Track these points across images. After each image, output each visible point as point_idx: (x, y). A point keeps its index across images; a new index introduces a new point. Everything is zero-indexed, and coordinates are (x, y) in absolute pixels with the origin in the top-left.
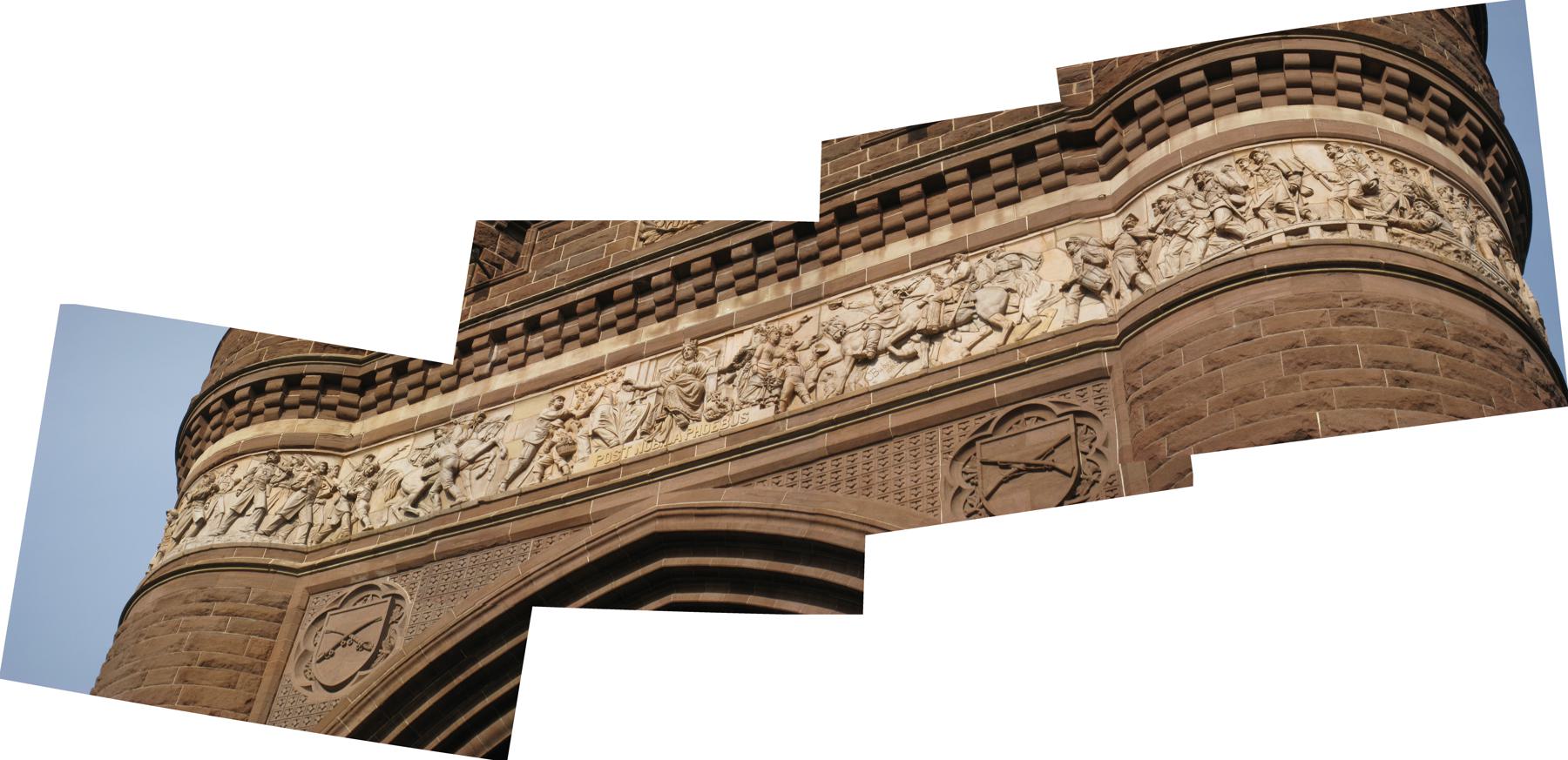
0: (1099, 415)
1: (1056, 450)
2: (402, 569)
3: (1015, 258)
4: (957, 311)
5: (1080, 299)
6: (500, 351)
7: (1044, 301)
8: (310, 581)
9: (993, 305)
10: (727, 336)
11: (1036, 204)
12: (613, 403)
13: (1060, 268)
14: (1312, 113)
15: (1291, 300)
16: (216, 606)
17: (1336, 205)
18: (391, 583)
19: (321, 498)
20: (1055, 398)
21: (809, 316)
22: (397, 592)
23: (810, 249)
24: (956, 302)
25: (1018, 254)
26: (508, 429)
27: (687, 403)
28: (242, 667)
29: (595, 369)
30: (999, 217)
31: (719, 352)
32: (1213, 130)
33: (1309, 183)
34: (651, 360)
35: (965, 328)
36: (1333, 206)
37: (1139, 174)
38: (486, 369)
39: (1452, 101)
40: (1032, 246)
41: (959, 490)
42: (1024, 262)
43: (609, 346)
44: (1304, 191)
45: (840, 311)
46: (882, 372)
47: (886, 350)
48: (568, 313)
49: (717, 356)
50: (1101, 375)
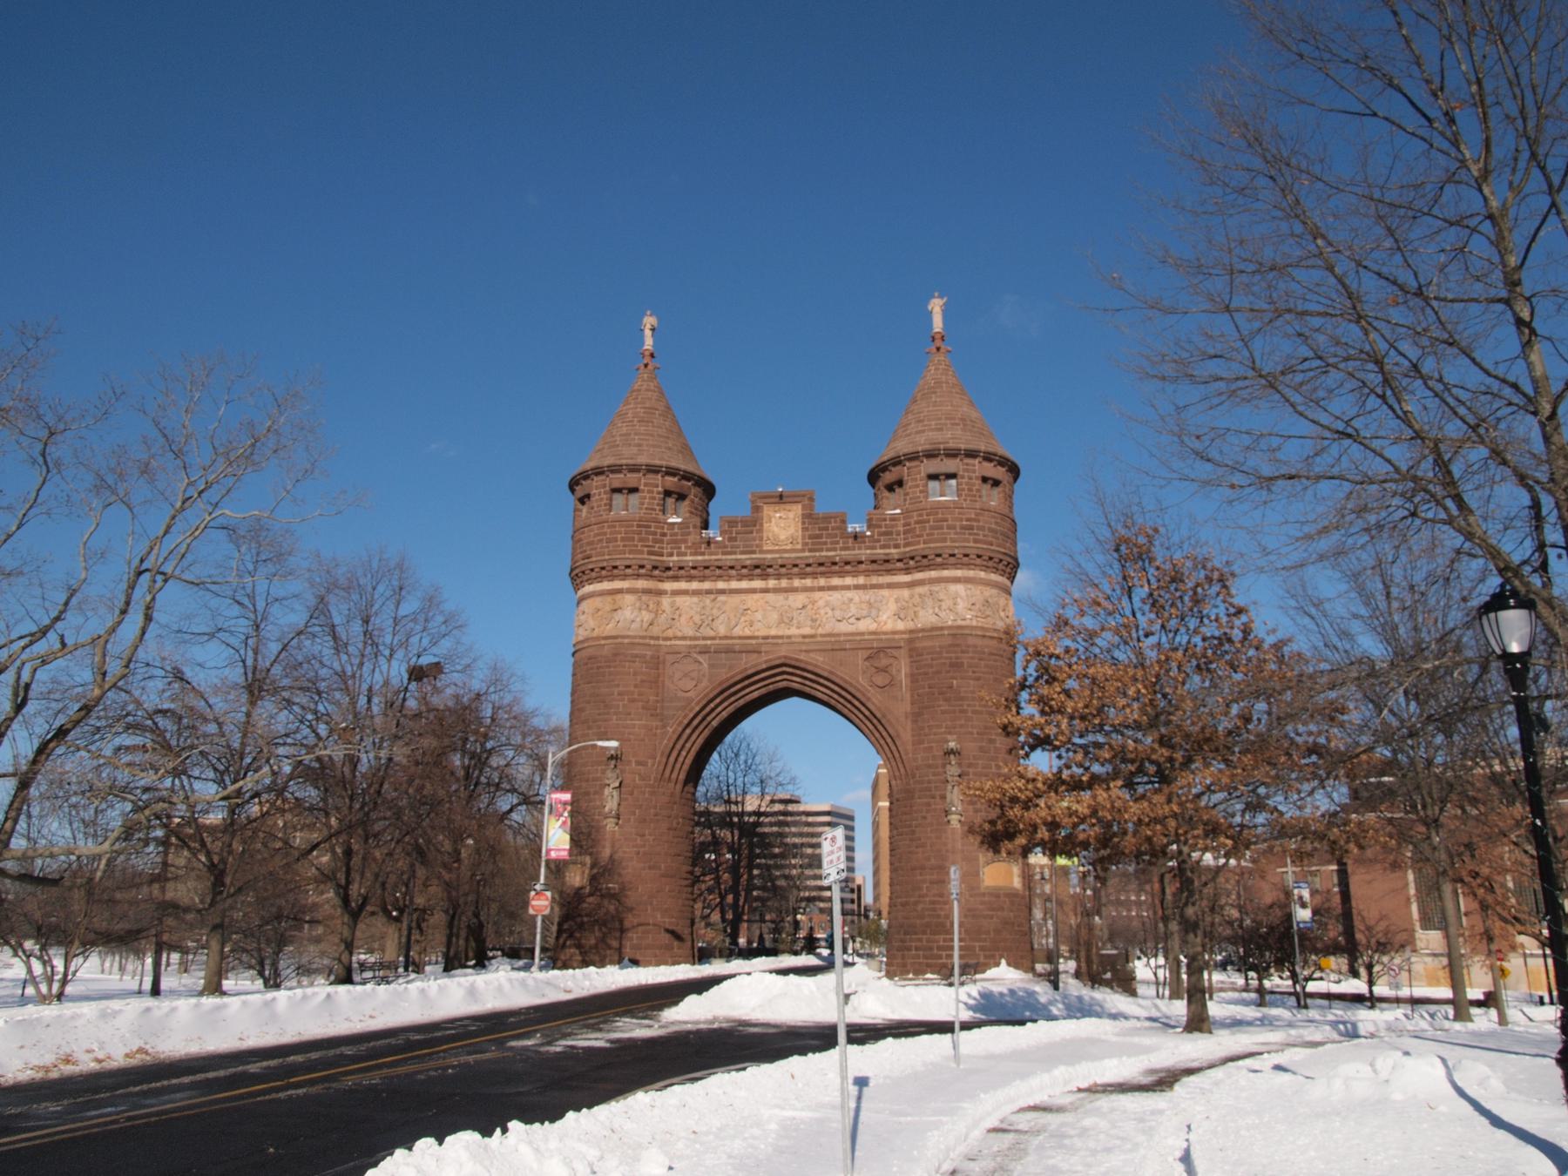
13: (893, 607)
29: (753, 591)
40: (885, 592)
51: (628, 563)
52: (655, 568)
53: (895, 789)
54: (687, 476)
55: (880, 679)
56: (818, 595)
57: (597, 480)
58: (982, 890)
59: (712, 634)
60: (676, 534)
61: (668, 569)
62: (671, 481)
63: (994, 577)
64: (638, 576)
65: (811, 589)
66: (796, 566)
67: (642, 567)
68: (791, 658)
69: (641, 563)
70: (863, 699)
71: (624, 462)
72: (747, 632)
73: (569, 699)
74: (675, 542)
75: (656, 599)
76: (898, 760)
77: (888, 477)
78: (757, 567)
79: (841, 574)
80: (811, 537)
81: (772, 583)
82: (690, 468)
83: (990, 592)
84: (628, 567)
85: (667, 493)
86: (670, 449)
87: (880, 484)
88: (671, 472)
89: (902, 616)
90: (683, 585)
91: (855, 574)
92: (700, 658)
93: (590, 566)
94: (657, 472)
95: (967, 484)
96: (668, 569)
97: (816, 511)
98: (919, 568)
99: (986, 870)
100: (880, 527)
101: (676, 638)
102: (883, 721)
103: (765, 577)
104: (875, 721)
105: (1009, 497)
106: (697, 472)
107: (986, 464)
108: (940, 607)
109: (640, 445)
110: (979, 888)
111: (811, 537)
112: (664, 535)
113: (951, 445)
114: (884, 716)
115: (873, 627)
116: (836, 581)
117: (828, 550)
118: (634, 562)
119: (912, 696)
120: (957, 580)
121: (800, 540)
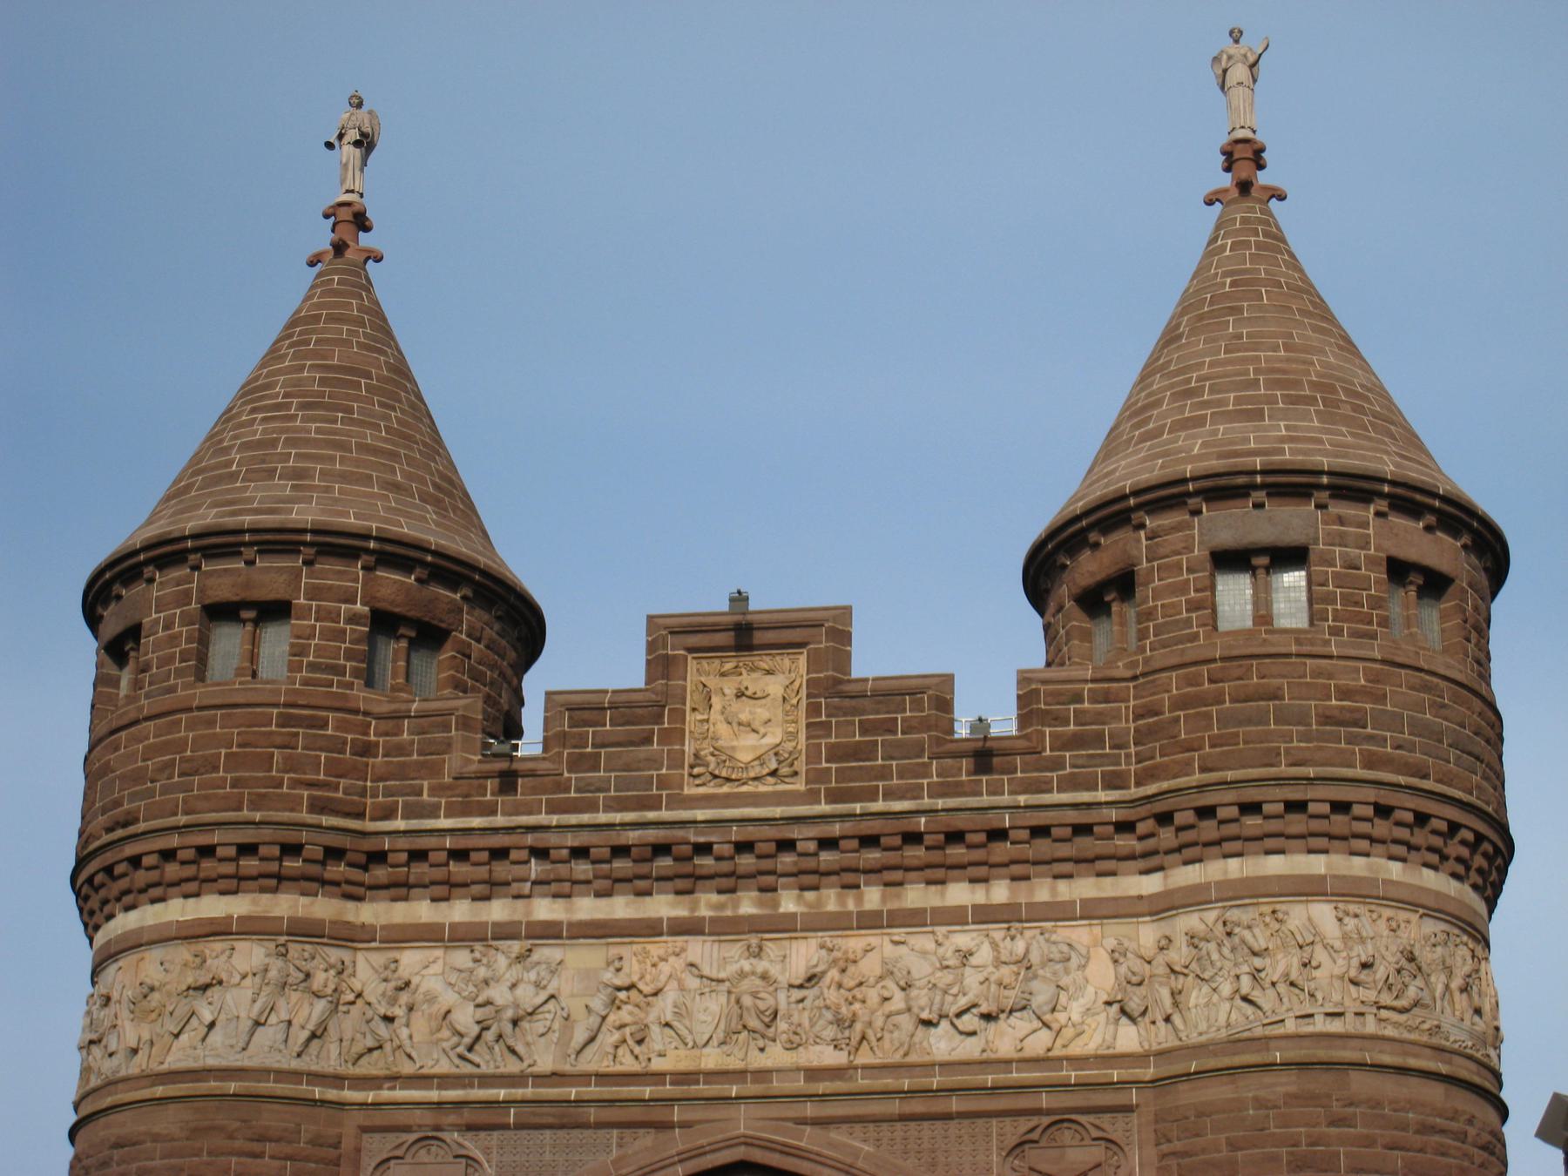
0: (1126, 1149)
1: (220, 881)
2: (471, 1128)
3: (1065, 948)
4: (1011, 997)
5: (1119, 1019)
6: (539, 869)
7: (1088, 1009)
9: (1046, 1003)
10: (791, 938)
12: (682, 988)
13: (1101, 977)
18: (460, 1140)
19: (345, 1004)
20: (1092, 1118)
21: (873, 945)
22: (471, 1154)
23: (873, 862)
24: (1014, 988)
25: (1069, 945)
27: (763, 1022)
30: (1053, 890)
31: (785, 957)
33: (1320, 955)
34: (714, 941)
35: (1017, 1014)
36: (1336, 985)
37: (1180, 889)
38: (527, 887)
39: (1494, 851)
40: (1080, 934)
42: (1073, 954)
43: (663, 906)
45: (903, 949)
47: (947, 1016)
48: (620, 851)
49: (783, 961)
50: (1128, 1109)
121: (801, 766)
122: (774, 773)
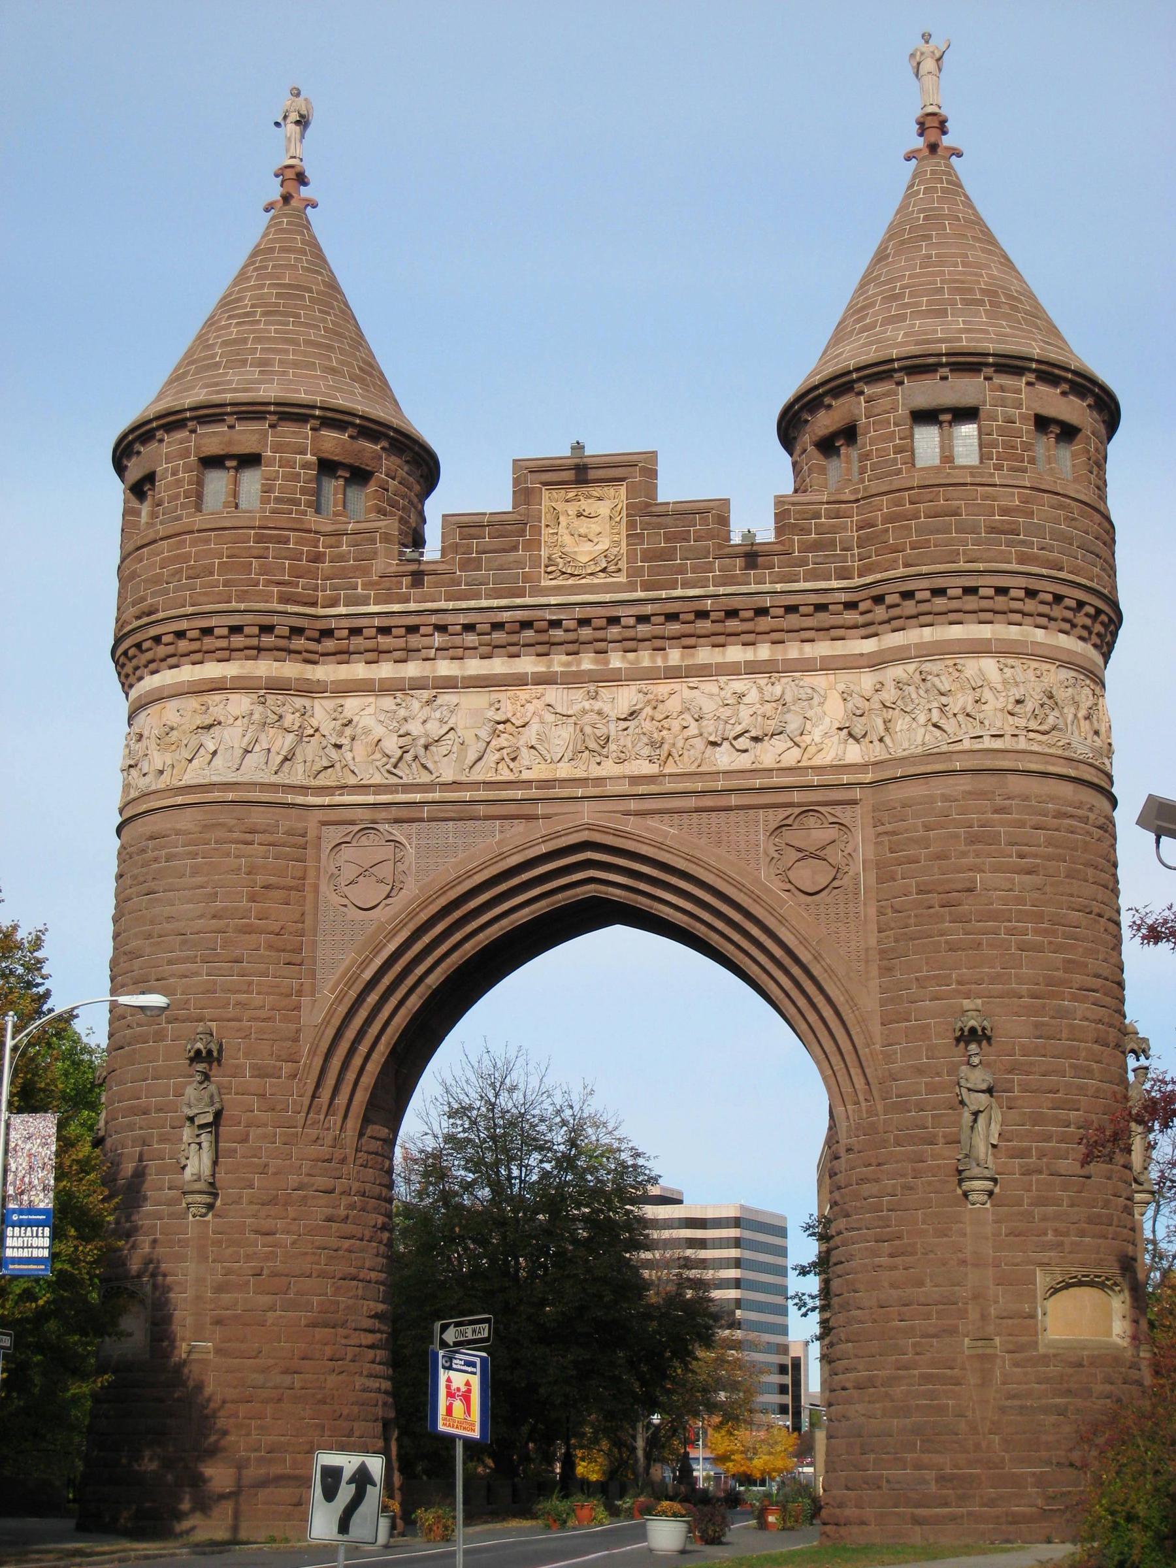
2: (397, 821)
3: (810, 691)
4: (771, 726)
8: (320, 815)
11: (823, 648)
13: (835, 711)
14: (993, 632)
15: (970, 793)
16: (257, 838)
17: (999, 714)
18: (390, 829)
20: (828, 809)
26: (459, 715)
28: (291, 888)
29: (520, 681)
32: (932, 635)
33: (987, 695)
40: (820, 681)
41: (773, 858)
42: (815, 695)
43: (528, 664)
44: (983, 701)
45: (696, 692)
46: (724, 758)
48: (497, 626)
51: (235, 620)
52: (296, 631)
53: (843, 1126)
54: (371, 429)
55: (808, 875)
56: (662, 688)
57: (172, 443)
58: (1042, 1350)
59: (425, 778)
60: (342, 558)
61: (328, 633)
62: (333, 442)
63: (1069, 643)
64: (259, 651)
65: (651, 675)
66: (614, 621)
67: (267, 629)
68: (604, 830)
69: (266, 620)
70: (771, 922)
71: (229, 397)
72: (505, 775)
73: (110, 928)
74: (342, 574)
75: (299, 702)
76: (850, 1058)
77: (824, 422)
78: (526, 625)
79: (720, 640)
80: (648, 556)
81: (558, 662)
82: (378, 412)
83: (1056, 676)
84: (236, 630)
85: (327, 467)
86: (333, 371)
87: (806, 439)
88: (334, 419)
89: (858, 731)
90: (358, 670)
91: (749, 639)
92: (398, 833)
93: (153, 631)
94: (302, 419)
95: (1002, 431)
96: (328, 633)
97: (661, 498)
98: (896, 623)
99: (1051, 1304)
100: (806, 531)
101: (343, 788)
102: (816, 970)
103: (545, 648)
104: (796, 971)
105: (1100, 463)
106: (395, 422)
107: (1042, 388)
108: (942, 708)
109: (263, 363)
110: (1035, 1344)
111: (648, 556)
112: (317, 558)
113: (964, 344)
114: (817, 958)
115: (791, 757)
116: (705, 655)
117: (686, 585)
118: (248, 618)
119: (881, 913)
120: (979, 649)
121: (623, 565)
122: (604, 570)
